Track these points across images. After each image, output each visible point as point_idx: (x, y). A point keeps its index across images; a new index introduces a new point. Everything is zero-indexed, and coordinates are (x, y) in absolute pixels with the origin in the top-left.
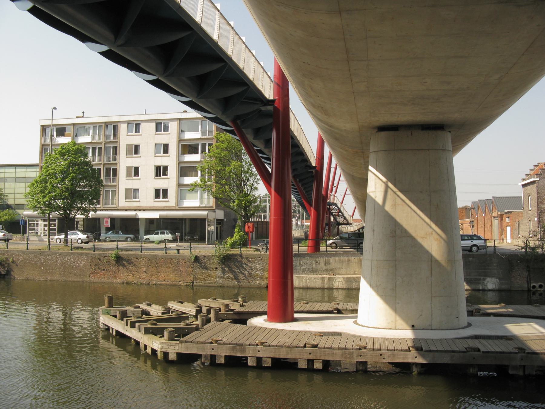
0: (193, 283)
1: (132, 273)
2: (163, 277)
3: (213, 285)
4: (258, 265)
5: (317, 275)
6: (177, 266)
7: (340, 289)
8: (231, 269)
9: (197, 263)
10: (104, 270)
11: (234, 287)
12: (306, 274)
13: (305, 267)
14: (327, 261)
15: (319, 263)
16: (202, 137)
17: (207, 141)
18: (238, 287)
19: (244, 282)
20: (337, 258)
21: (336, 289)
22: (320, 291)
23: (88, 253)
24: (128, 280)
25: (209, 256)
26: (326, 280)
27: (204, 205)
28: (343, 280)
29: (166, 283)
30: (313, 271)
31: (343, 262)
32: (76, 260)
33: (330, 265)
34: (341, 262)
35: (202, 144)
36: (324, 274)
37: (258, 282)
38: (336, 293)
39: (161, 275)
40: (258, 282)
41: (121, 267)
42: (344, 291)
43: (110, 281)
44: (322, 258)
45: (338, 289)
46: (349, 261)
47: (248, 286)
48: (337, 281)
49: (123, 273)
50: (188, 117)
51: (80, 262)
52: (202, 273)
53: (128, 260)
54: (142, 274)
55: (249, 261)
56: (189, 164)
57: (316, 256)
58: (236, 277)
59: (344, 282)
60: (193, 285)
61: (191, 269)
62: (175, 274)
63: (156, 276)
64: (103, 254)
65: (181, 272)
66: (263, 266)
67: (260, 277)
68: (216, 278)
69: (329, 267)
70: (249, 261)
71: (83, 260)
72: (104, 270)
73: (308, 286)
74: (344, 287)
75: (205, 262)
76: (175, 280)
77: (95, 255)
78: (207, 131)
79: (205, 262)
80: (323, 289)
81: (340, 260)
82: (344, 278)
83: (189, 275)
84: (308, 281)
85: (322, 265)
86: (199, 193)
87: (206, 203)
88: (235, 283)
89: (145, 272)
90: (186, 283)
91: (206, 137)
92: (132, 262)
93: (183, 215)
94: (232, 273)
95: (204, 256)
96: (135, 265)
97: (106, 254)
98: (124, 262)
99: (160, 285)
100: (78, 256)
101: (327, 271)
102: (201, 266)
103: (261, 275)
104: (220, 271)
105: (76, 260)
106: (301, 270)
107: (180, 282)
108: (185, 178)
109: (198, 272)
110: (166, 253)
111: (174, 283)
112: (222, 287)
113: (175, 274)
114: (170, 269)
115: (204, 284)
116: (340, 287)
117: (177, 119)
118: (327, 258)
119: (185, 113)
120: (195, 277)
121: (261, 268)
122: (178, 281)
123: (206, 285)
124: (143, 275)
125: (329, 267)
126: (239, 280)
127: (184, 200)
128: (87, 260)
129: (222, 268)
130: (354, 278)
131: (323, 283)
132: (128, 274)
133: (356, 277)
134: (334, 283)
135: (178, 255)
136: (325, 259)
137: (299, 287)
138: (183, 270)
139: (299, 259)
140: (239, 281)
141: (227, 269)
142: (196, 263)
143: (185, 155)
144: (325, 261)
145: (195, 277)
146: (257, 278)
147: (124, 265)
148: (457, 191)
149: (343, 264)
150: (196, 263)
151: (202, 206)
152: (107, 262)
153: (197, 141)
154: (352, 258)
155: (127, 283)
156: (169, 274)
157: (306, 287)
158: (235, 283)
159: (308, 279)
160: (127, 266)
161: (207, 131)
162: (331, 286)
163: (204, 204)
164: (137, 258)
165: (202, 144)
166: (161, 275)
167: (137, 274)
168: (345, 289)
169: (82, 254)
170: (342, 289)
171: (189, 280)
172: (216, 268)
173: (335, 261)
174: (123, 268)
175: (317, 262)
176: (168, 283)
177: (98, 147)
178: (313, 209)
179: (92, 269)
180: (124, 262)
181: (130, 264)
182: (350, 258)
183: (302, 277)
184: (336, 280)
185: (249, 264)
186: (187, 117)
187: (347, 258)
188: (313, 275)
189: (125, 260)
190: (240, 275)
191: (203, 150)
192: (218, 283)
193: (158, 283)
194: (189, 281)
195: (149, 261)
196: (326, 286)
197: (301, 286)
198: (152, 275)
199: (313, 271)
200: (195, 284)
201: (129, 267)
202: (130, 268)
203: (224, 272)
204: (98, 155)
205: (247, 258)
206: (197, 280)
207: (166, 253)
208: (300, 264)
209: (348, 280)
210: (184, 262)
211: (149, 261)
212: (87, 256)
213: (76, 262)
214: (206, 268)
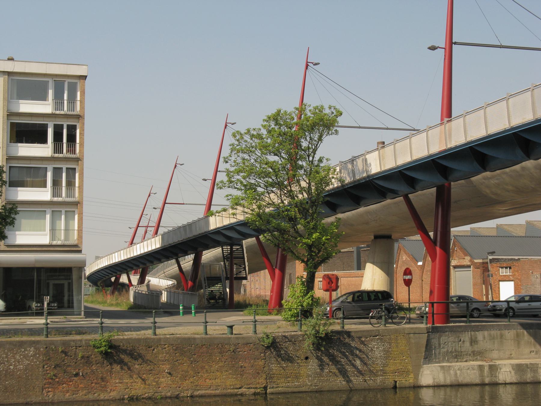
0: (265, 388)
1: (141, 378)
2: (208, 380)
3: (303, 389)
4: (377, 348)
5: (461, 362)
6: (234, 359)
7: (508, 384)
8: (333, 359)
9: (272, 350)
10: (77, 375)
11: (340, 391)
12: (448, 361)
13: (446, 350)
14: (473, 338)
15: (464, 341)
16: (54, 112)
17: (66, 120)
18: (349, 390)
19: (357, 381)
20: (486, 333)
21: (503, 384)
22: (478, 388)
23: (38, 342)
24: (133, 393)
25: (292, 336)
26: (486, 369)
27: (59, 243)
28: (511, 369)
29: (213, 392)
30: (456, 357)
31: (494, 338)
32: (6, 357)
33: (477, 344)
34: (492, 338)
35: (54, 124)
36: (470, 360)
37: (379, 379)
38: (501, 389)
39: (202, 376)
40: (379, 379)
41: (117, 368)
42: (514, 387)
43: (91, 397)
44: (466, 332)
45: (506, 384)
46: (502, 336)
47: (363, 388)
48: (502, 370)
49: (120, 379)
50: (27, 71)
51: (19, 362)
52: (283, 369)
53: (131, 351)
54: (163, 377)
55: (362, 343)
56: (28, 162)
57: (460, 330)
58: (343, 373)
59: (513, 372)
60: (266, 393)
61: (261, 363)
62: (230, 374)
63: (192, 380)
64: (74, 341)
65: (243, 369)
66: (384, 350)
67: (381, 370)
68: (309, 376)
69: (476, 348)
70: (362, 343)
71: (26, 357)
72: (77, 375)
73: (460, 381)
74: (514, 380)
75: (286, 348)
76: (230, 386)
77: (53, 344)
78: (66, 102)
79: (286, 348)
80: (483, 385)
81: (490, 335)
82: (512, 365)
83: (258, 373)
84: (458, 372)
85: (467, 344)
86: (48, 217)
87: (63, 238)
88: (340, 382)
89: (170, 374)
90: (253, 391)
91: (62, 112)
92: (140, 356)
93: (37, 261)
94: (336, 365)
95: (284, 336)
96: (145, 361)
97: (81, 341)
98: (122, 356)
99: (201, 396)
100: (13, 349)
101: (474, 354)
102: (279, 356)
103: (383, 367)
104: (313, 364)
105: (6, 357)
106: (441, 354)
107: (240, 388)
108: (19, 189)
109: (274, 367)
110: (155, 334)
111: (229, 391)
112: (319, 392)
113: (230, 374)
114: (221, 364)
115: (286, 389)
116: (508, 381)
117: (4, 72)
118: (473, 333)
119: (11, 62)
120: (270, 377)
121: (382, 353)
122: (238, 386)
123: (290, 390)
124: (165, 380)
125: (476, 348)
126: (348, 377)
127: (17, 233)
128: (34, 356)
129: (318, 358)
130: (527, 365)
131: (482, 375)
132: (132, 381)
133: (531, 364)
134: (499, 374)
135: (154, 337)
136: (471, 334)
137: (445, 384)
138: (246, 365)
139: (437, 335)
140: (349, 381)
141: (325, 359)
142: (270, 350)
143: (20, 145)
144: (471, 338)
145: (270, 377)
146: (377, 371)
147: (121, 362)
148: (494, 220)
149: (494, 342)
150: (270, 350)
151: (54, 243)
152: (83, 357)
153: (45, 119)
154: (507, 331)
155: (131, 399)
156: (218, 374)
157: (456, 383)
158: (340, 382)
159: (459, 369)
160: (129, 364)
161: (66, 102)
162: (494, 380)
163: (59, 240)
164: (149, 344)
165: (54, 124)
166: (202, 376)
167: (151, 378)
168: (516, 383)
169: (21, 344)
170: (511, 384)
171: (259, 383)
172: (307, 358)
173: (484, 338)
174: (122, 368)
175: (460, 341)
176: (218, 392)
177: (68, 126)
178: (438, 249)
179: (49, 375)
180: (122, 356)
181: (136, 359)
182: (503, 332)
183: (449, 366)
184: (500, 369)
185: (362, 347)
186: (27, 71)
187: (499, 332)
188: (457, 362)
189: (125, 351)
190: (349, 368)
191: (58, 137)
192: (311, 385)
193: (197, 393)
194: (258, 386)
195: (176, 350)
196: (487, 381)
197: (448, 382)
198: (184, 378)
199: (457, 356)
200: (269, 391)
201: (135, 364)
202: (137, 366)
203: (322, 366)
204: (68, 140)
205: (360, 338)
206: (274, 382)
207: (155, 334)
208: (440, 344)
209: (519, 368)
210: (246, 349)
211: (176, 350)
212: (35, 348)
213: (7, 361)
214: (289, 359)
